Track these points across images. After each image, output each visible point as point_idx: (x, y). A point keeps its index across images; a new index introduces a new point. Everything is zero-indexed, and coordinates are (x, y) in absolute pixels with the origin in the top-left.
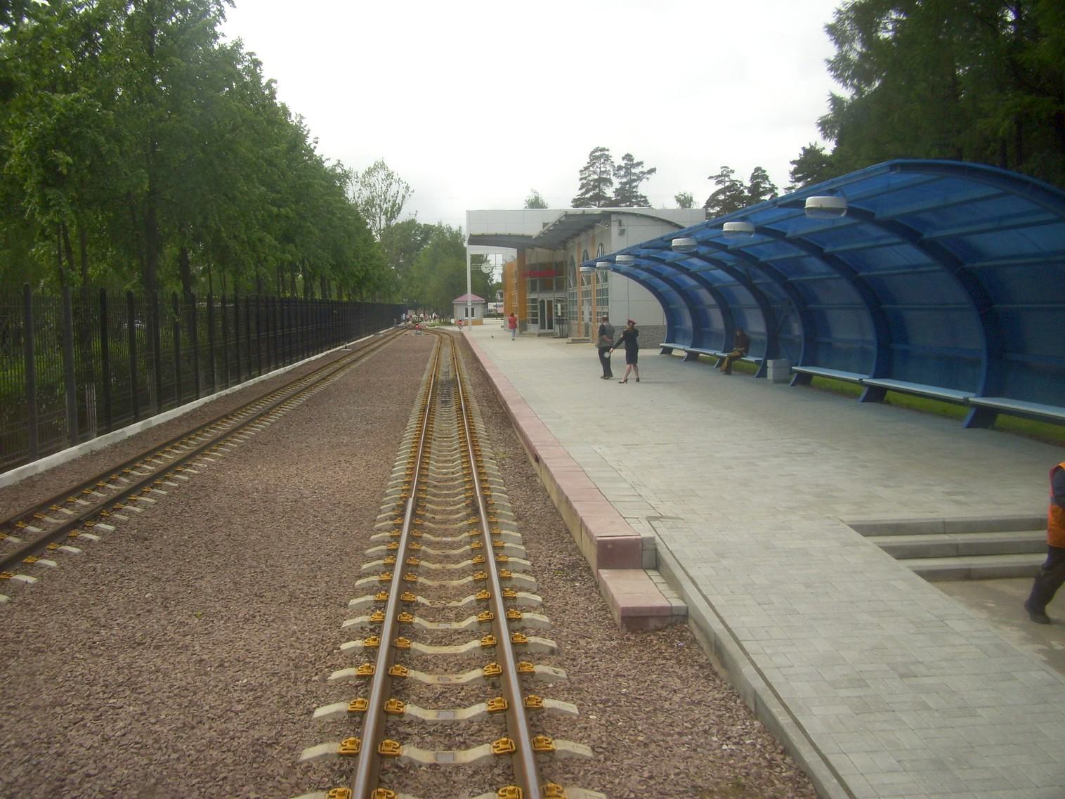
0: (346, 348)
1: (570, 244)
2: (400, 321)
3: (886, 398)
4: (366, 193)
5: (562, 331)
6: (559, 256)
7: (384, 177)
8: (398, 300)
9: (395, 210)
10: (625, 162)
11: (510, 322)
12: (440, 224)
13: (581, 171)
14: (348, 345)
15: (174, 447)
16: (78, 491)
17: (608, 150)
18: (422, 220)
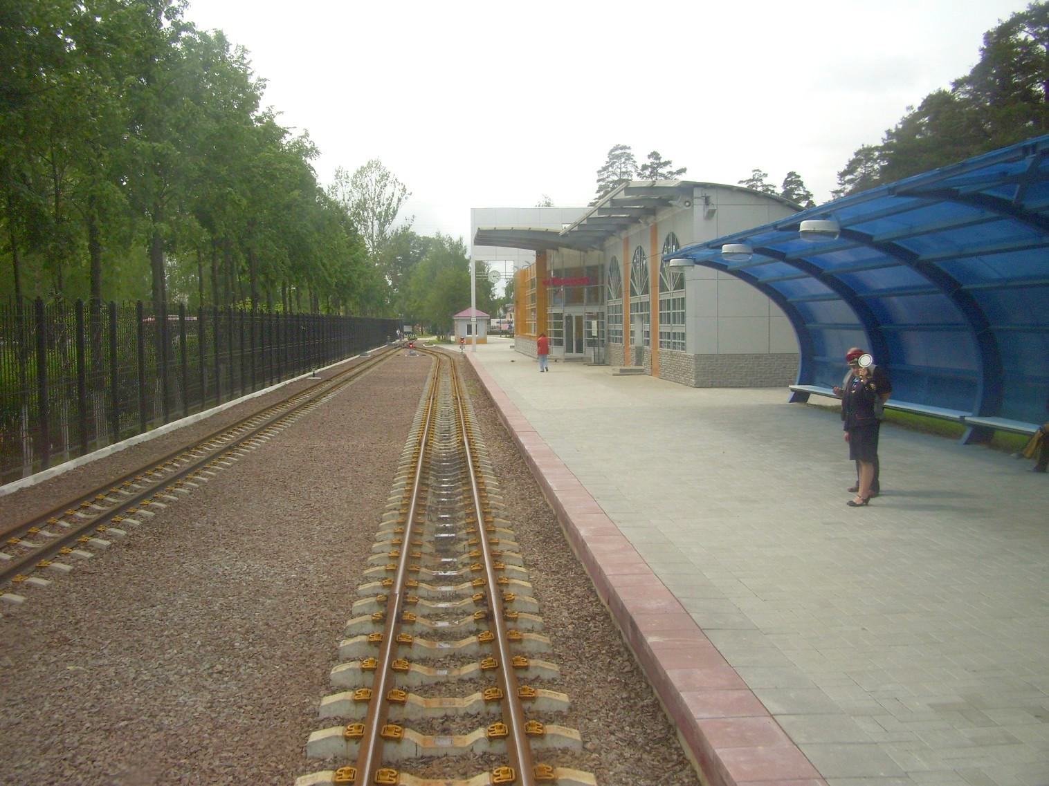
1: (607, 244)
2: (395, 337)
3: (793, 393)
4: (357, 196)
5: (597, 356)
6: (594, 258)
7: (378, 178)
8: (395, 314)
9: (387, 216)
10: (652, 160)
11: (539, 345)
12: (438, 234)
13: (599, 172)
14: (316, 372)
17: (629, 148)
18: (423, 230)
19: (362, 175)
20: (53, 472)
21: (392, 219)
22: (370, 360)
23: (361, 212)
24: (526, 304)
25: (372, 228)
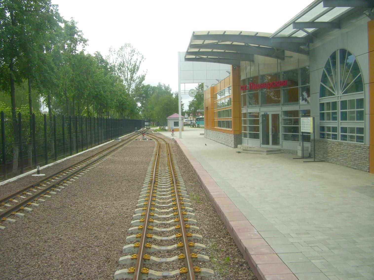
0: (38, 172)
4: (120, 60)
9: (133, 71)
15: (80, 164)
16: (21, 192)
19: (122, 51)
20: (56, 162)
21: (137, 71)
22: (120, 142)
23: (122, 68)
24: (214, 109)
25: (127, 76)
